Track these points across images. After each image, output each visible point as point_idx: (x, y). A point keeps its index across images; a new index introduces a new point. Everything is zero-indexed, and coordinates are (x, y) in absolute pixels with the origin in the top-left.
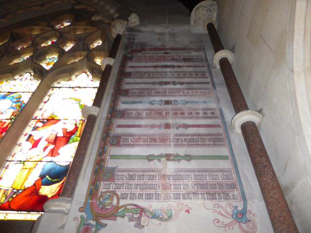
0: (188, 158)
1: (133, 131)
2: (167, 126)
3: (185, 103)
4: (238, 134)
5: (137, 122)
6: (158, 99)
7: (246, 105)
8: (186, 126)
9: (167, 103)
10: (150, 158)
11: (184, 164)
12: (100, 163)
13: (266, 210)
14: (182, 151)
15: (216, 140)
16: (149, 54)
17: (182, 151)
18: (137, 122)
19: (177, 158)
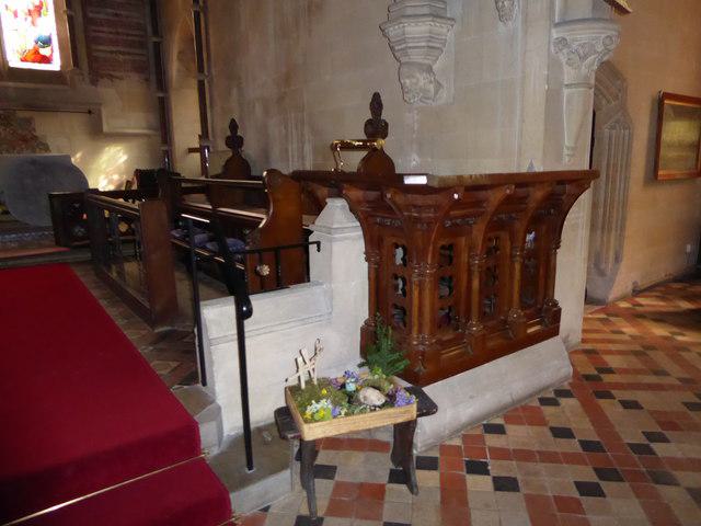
0: (129, 54)
1: (101, 35)
2: (118, 33)
3: (316, 417)
4: (223, 152)
5: (101, 28)
6: (110, 11)
7: (577, 487)
8: (128, 35)
9: (116, 15)
10: (112, 52)
11: (127, 57)
12: (89, 55)
13: (272, 294)
14: (126, 50)
15: (142, 45)
16: (650, 313)
17: (126, 50)
18: (101, 28)
19: (123, 53)
